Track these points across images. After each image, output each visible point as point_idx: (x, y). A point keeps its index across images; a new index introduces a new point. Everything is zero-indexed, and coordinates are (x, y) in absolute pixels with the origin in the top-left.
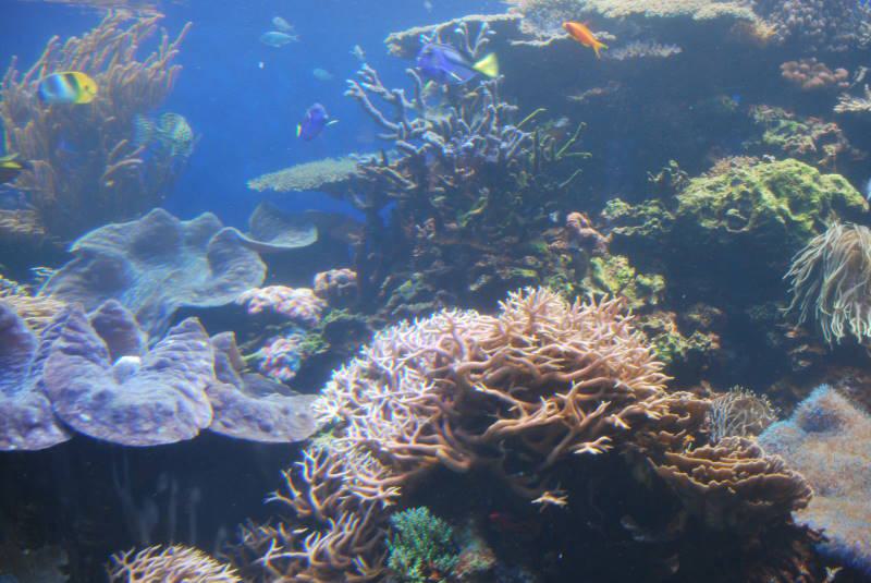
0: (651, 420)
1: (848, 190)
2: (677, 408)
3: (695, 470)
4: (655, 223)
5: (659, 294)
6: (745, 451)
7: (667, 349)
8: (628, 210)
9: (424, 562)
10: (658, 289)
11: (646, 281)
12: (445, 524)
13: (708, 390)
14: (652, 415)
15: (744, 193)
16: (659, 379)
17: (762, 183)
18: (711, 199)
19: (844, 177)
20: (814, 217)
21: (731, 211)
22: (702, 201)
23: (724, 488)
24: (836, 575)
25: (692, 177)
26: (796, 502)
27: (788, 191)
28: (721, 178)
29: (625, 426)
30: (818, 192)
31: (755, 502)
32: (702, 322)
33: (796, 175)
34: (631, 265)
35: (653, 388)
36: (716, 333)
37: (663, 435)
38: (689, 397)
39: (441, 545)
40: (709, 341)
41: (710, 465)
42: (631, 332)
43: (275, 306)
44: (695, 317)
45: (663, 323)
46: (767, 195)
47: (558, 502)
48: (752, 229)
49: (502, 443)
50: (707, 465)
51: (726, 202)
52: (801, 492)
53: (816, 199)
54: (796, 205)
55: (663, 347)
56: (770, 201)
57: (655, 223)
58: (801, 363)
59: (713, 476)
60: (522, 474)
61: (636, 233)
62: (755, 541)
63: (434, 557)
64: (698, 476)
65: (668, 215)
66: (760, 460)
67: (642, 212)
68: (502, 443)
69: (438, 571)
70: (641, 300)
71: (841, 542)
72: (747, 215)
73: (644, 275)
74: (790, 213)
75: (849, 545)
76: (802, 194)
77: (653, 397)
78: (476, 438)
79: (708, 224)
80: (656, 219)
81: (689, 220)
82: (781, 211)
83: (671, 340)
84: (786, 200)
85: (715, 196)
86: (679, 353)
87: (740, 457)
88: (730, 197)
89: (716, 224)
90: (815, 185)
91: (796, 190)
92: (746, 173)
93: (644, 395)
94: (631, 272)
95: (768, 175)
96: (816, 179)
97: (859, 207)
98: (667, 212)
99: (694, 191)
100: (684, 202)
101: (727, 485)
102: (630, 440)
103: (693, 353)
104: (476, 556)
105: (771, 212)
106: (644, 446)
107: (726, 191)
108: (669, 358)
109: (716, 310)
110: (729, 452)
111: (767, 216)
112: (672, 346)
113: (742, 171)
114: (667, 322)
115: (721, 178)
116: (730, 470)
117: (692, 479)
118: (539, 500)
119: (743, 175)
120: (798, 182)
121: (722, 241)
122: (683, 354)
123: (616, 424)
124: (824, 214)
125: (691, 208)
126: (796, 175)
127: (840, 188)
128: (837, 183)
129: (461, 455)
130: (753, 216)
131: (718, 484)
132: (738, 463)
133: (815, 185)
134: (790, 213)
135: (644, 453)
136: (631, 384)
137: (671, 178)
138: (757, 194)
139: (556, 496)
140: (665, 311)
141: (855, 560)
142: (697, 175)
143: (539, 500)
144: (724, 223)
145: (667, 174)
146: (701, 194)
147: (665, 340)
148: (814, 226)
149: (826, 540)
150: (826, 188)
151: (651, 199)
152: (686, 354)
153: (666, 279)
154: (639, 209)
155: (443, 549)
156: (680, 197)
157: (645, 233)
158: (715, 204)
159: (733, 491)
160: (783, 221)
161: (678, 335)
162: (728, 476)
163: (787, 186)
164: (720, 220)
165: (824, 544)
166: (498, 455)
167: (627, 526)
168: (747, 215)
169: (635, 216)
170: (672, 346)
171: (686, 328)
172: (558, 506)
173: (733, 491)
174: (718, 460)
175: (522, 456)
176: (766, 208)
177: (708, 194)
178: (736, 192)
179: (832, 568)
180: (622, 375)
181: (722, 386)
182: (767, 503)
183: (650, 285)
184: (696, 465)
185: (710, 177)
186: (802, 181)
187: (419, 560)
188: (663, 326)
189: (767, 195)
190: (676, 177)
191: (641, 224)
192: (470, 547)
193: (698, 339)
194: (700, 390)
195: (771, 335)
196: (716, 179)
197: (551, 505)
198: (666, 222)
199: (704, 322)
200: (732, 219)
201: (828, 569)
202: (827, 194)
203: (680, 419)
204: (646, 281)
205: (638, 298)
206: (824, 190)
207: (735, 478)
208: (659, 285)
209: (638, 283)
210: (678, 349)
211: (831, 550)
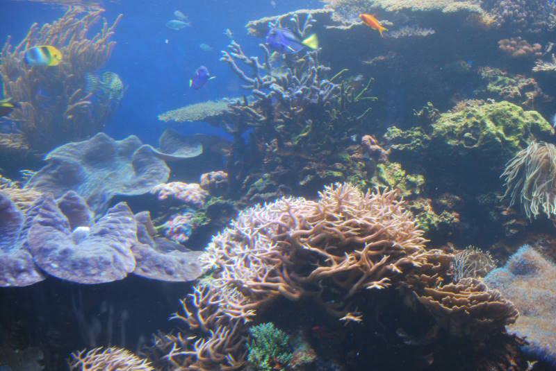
0: (416, 267)
1: (542, 121)
2: (432, 260)
3: (444, 299)
4: (418, 142)
5: (421, 187)
6: (476, 287)
7: (426, 222)
8: (401, 134)
9: (271, 358)
10: (420, 184)
11: (412, 179)
12: (284, 333)
13: (452, 248)
14: (416, 264)
15: (475, 123)
16: (420, 241)
17: (486, 117)
18: (454, 127)
19: (539, 112)
20: (519, 138)
21: (467, 135)
22: (448, 128)
23: (462, 311)
24: (534, 366)
25: (442, 112)
26: (508, 319)
27: (503, 122)
28: (460, 113)
29: (399, 271)
30: (522, 122)
31: (482, 319)
32: (448, 205)
33: (508, 111)
34: (403, 169)
35: (417, 247)
36: (457, 212)
37: (423, 277)
38: (440, 253)
39: (282, 347)
40: (453, 217)
41: (453, 296)
42: (403, 211)
43: (176, 195)
44: (444, 201)
45: (424, 206)
46: (489, 124)
47: (356, 319)
48: (480, 146)
49: (320, 282)
50: (452, 296)
51: (463, 129)
52: (511, 313)
53: (521, 127)
54: (508, 131)
55: (423, 221)
56: (491, 128)
57: (418, 142)
58: (511, 231)
59: (455, 303)
60: (333, 301)
61: (406, 148)
62: (482, 344)
63: (277, 354)
64: (446, 303)
65: (427, 137)
66: (485, 293)
67: (410, 135)
68: (320, 282)
69: (280, 363)
70: (409, 191)
71: (537, 345)
72: (477, 137)
73: (411, 175)
74: (504, 136)
75: (542, 347)
76: (512, 123)
77: (417, 253)
78: (304, 279)
79: (452, 142)
80: (419, 140)
81: (440, 140)
82: (498, 135)
83: (428, 217)
84: (502, 127)
85: (456, 125)
86: (433, 225)
87: (472, 291)
88: (466, 125)
89: (457, 143)
90: (520, 118)
91: (508, 121)
92: (476, 110)
93: (411, 251)
94: (403, 173)
95: (490, 111)
96: (521, 114)
97: (549, 132)
98: (426, 135)
99: (443, 122)
100: (437, 128)
101: (464, 309)
102: (402, 280)
103: (442, 225)
104: (304, 354)
105: (492, 135)
106: (411, 284)
107: (463, 121)
108: (427, 228)
109: (457, 197)
110: (465, 288)
111: (490, 138)
112: (429, 220)
113: (473, 109)
114: (426, 205)
115: (460, 113)
116: (466, 299)
117: (442, 305)
118: (344, 318)
119: (474, 111)
120: (509, 116)
121: (461, 154)
122: (436, 225)
123: (393, 270)
124: (526, 136)
125: (441, 132)
126: (508, 111)
127: (536, 120)
128: (535, 116)
129: (294, 289)
130: (481, 137)
131: (459, 308)
132: (471, 295)
133: (520, 118)
134: (504, 136)
135: (411, 288)
136: (403, 245)
137: (429, 113)
138: (483, 124)
139: (355, 316)
140: (425, 198)
141: (546, 356)
142: (445, 111)
143: (344, 318)
144: (462, 142)
145: (426, 111)
146: (447, 124)
147: (425, 216)
148: (520, 144)
149: (527, 343)
150: (528, 119)
151: (415, 127)
152: (438, 225)
153: (425, 177)
154: (408, 133)
155: (283, 350)
156: (434, 126)
157: (412, 148)
158: (457, 130)
159: (468, 313)
160: (500, 141)
161: (433, 213)
162: (465, 303)
163: (502, 119)
164: (460, 140)
165: (526, 346)
166: (318, 289)
167: (401, 335)
168: (477, 137)
169: (405, 137)
170: (429, 220)
171: (438, 209)
172: (356, 322)
173: (468, 313)
174: (458, 293)
175: (333, 290)
176: (489, 133)
177: (452, 123)
178: (470, 122)
179: (531, 361)
180: (397, 239)
181: (461, 246)
182: (490, 320)
183: (415, 181)
184: (445, 296)
185: (453, 113)
186: (512, 115)
187: (268, 356)
188: (423, 208)
189: (489, 124)
190: (432, 113)
191: (409, 142)
192: (300, 348)
193: (445, 216)
194: (447, 248)
195: (492, 213)
196: (457, 114)
197: (352, 321)
198: (425, 142)
199: (449, 205)
200: (467, 139)
201: (528, 362)
202: (528, 124)
203: (434, 267)
204: (412, 179)
205: (407, 189)
206: (526, 121)
207: (469, 304)
208: (421, 181)
209: (407, 180)
210: (433, 222)
211: (530, 350)
